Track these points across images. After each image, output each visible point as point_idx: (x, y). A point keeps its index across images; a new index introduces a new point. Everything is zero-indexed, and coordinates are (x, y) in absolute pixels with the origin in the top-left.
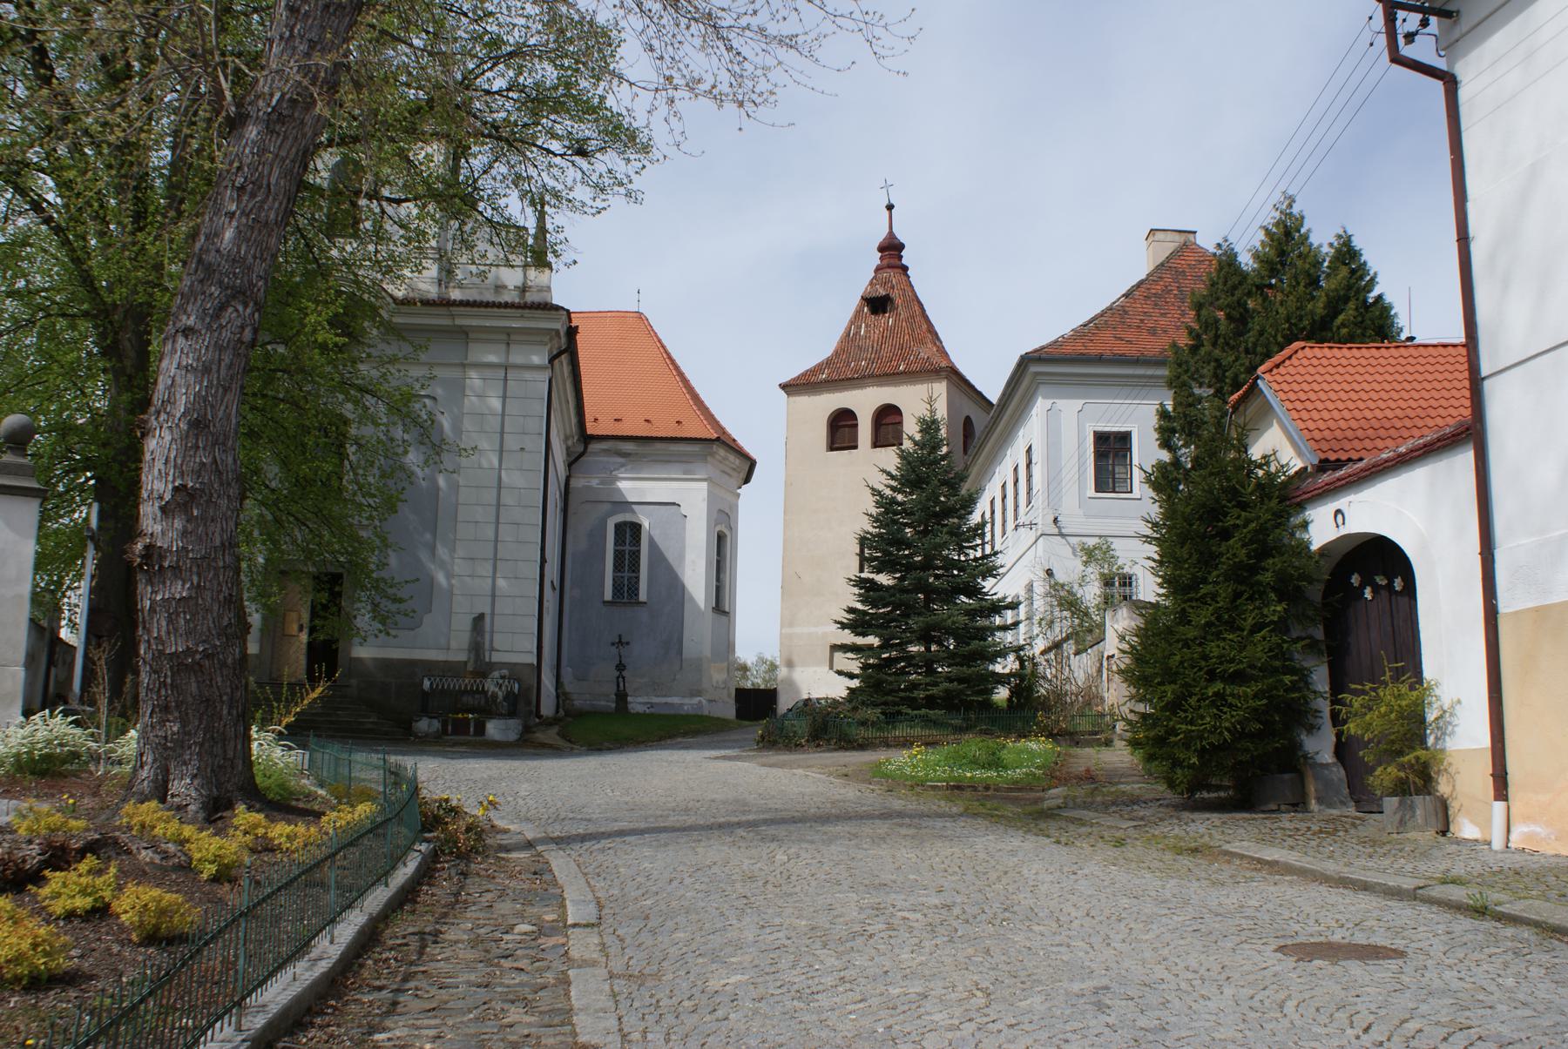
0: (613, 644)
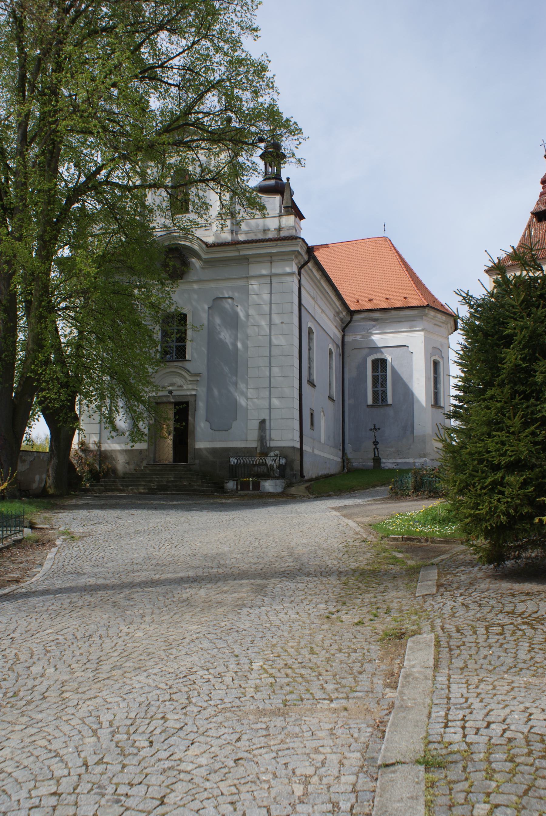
0: (371, 430)
